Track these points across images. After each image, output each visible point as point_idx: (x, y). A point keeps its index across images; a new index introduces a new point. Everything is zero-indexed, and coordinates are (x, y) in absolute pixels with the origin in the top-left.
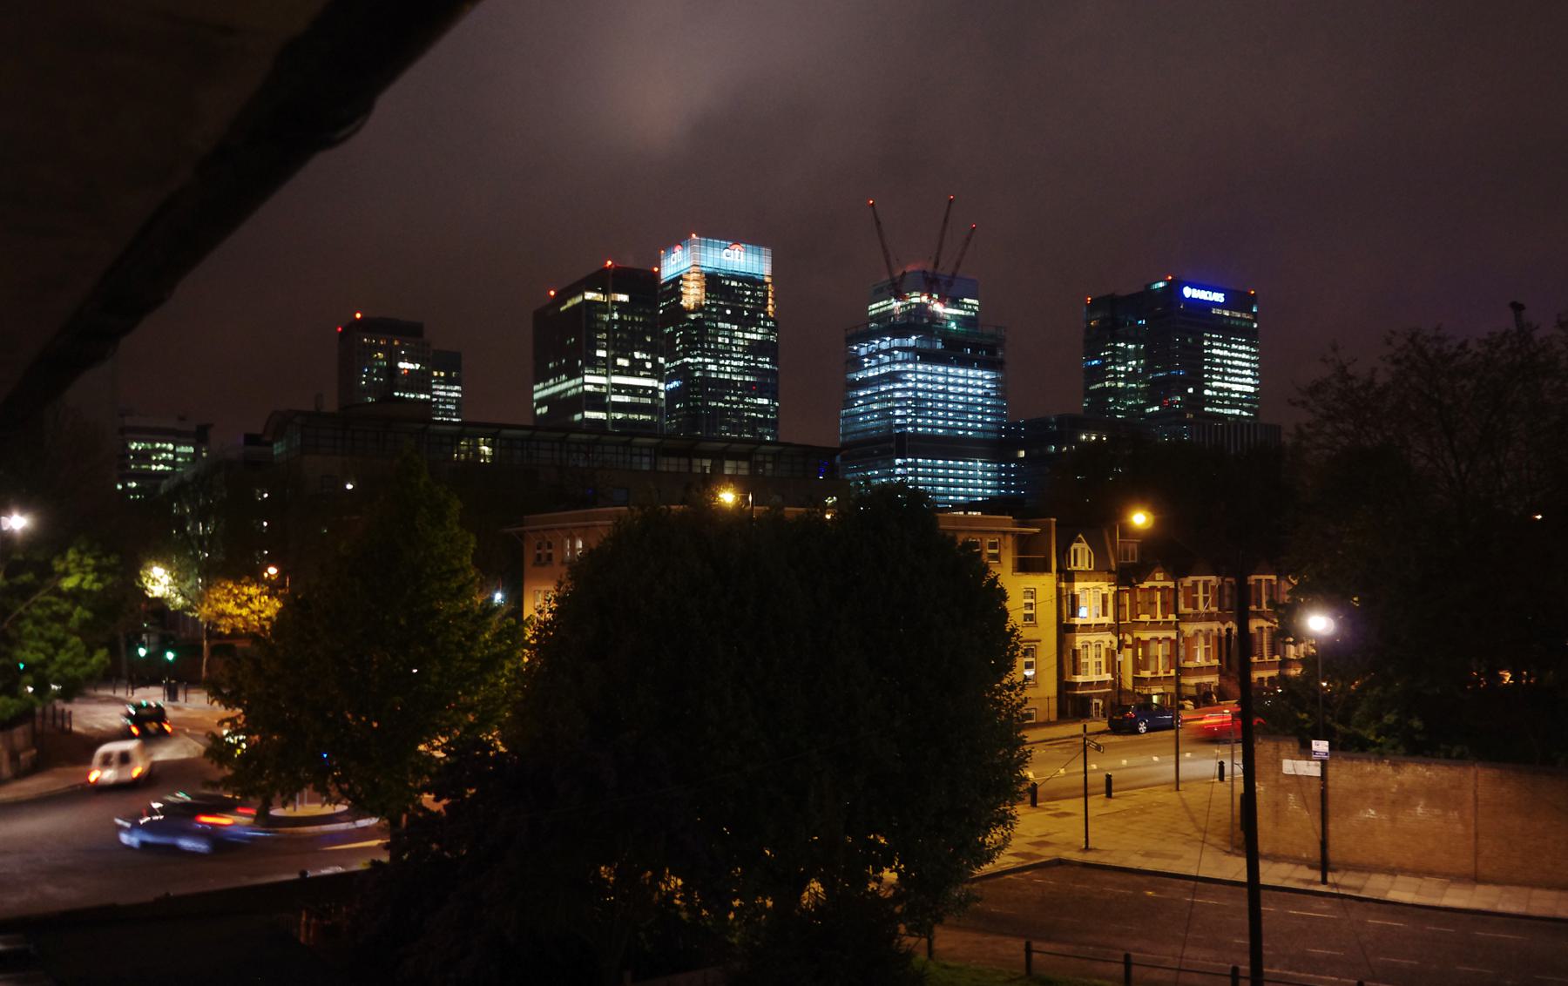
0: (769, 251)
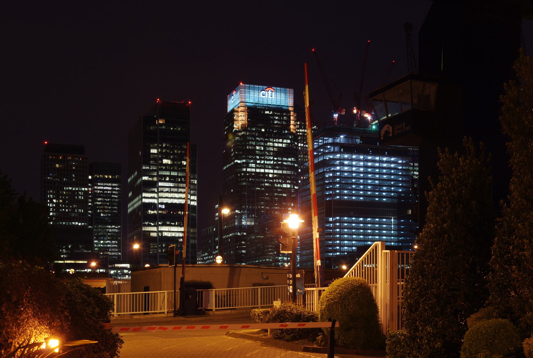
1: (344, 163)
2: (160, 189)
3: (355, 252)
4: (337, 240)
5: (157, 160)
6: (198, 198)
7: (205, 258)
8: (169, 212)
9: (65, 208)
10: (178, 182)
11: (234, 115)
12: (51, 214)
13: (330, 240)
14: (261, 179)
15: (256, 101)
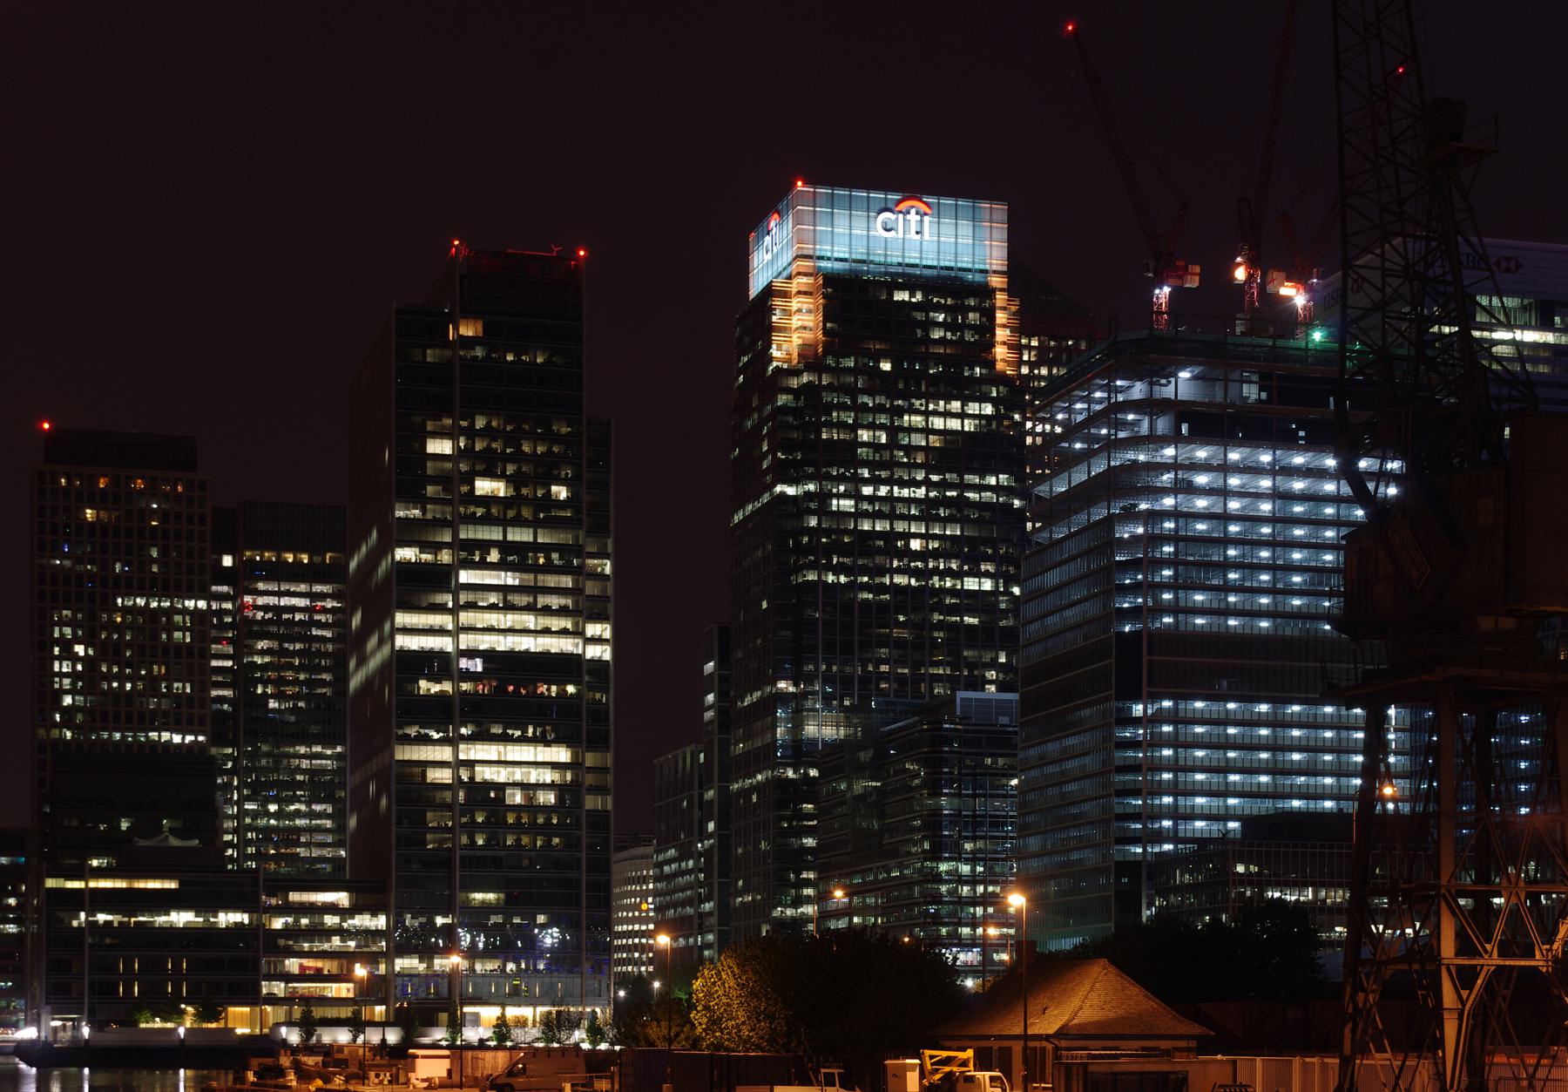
1: (1190, 483)
2: (464, 597)
3: (1234, 841)
5: (455, 480)
6: (615, 631)
7: (666, 869)
9: (122, 678)
10: (536, 569)
12: (68, 700)
13: (1136, 793)
14: (879, 560)
15: (860, 252)
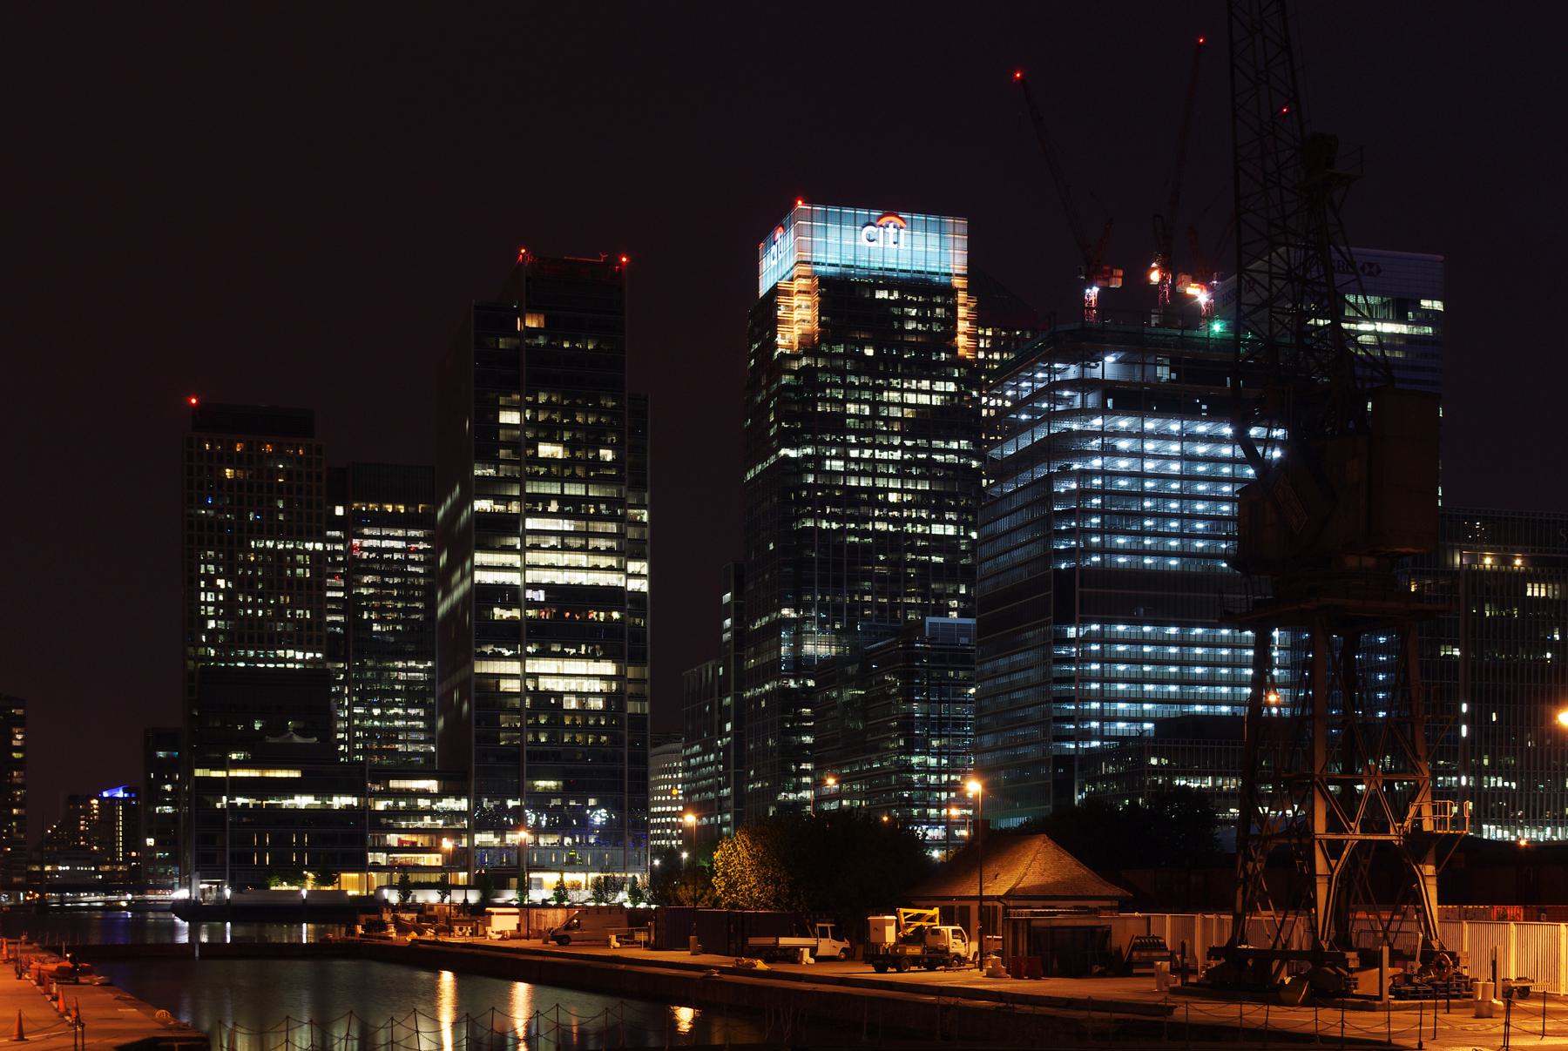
0: (962, 224)
2: (529, 541)
3: (1149, 739)
4: (1090, 701)
5: (522, 444)
6: (651, 568)
8: (560, 615)
9: (255, 607)
10: (588, 518)
11: (776, 306)
12: (212, 624)
13: (1070, 700)
14: (863, 510)
15: (848, 259)
